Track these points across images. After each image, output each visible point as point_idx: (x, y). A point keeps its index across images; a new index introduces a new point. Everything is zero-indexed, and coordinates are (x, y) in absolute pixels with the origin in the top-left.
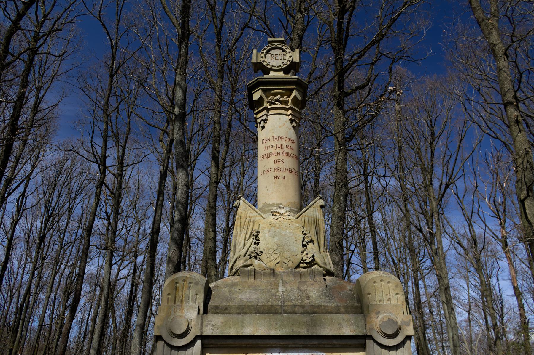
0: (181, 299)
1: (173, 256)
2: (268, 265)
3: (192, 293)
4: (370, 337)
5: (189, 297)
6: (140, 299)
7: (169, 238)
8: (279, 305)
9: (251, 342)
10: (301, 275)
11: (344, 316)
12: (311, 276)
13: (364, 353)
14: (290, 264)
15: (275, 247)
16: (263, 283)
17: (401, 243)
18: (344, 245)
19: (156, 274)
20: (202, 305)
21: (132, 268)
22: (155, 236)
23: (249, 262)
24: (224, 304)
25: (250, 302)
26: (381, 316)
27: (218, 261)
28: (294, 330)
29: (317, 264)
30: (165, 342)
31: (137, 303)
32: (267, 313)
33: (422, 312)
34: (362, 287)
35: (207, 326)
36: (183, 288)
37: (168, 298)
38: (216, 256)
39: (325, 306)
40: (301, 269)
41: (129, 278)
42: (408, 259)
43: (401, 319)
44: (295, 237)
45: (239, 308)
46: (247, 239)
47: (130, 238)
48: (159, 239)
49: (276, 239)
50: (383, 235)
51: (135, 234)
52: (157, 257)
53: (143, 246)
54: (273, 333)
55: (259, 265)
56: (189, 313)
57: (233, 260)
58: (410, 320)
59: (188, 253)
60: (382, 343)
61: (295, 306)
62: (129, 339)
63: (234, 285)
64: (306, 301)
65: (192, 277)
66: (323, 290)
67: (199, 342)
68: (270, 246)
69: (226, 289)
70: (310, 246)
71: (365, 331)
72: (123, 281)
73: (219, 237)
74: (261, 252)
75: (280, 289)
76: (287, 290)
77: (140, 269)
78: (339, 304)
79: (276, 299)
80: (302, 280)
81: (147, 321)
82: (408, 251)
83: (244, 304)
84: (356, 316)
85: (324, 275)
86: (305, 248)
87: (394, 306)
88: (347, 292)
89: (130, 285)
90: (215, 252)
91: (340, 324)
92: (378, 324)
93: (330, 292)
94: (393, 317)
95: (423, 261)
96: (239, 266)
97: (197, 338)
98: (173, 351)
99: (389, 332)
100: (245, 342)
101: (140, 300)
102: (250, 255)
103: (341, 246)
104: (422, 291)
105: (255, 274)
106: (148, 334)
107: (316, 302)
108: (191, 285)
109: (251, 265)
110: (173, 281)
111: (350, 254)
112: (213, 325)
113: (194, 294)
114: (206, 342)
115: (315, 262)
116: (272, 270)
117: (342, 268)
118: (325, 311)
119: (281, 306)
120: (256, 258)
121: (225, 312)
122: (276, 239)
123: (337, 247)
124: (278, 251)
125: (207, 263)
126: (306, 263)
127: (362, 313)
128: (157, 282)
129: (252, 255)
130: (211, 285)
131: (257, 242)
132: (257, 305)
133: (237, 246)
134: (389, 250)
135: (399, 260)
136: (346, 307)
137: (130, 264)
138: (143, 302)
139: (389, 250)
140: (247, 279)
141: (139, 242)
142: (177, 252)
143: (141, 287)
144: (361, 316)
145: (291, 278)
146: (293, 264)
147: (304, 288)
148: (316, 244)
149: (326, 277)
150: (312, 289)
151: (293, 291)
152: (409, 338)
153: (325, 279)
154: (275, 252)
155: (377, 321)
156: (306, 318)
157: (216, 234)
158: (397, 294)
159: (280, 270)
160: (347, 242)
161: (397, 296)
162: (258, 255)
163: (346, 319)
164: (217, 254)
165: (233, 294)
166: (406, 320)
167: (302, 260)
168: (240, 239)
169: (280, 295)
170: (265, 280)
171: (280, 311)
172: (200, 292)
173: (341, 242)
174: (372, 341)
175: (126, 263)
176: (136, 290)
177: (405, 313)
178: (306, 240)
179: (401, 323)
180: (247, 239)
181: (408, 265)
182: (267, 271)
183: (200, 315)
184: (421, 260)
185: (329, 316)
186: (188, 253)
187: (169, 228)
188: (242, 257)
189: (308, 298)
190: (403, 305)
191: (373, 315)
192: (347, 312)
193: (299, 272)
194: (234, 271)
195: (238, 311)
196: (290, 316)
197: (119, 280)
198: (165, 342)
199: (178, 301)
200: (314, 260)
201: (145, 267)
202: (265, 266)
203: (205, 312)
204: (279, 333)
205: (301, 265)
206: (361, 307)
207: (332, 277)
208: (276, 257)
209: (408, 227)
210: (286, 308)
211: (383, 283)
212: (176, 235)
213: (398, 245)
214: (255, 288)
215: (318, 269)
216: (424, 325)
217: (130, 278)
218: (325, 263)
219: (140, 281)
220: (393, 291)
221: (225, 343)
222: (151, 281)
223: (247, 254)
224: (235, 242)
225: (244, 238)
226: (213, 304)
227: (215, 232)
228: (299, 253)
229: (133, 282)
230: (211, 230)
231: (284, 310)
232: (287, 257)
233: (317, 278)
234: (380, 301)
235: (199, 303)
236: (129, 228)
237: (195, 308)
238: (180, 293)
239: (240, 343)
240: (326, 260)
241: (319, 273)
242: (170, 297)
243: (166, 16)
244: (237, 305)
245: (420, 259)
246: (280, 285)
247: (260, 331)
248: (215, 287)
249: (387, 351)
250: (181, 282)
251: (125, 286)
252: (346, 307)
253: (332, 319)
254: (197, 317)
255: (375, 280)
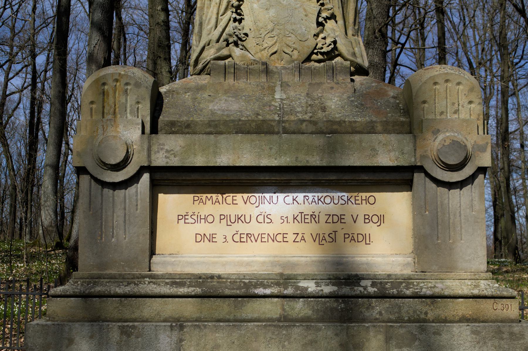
0: (112, 110)
1: (96, 51)
2: (257, 57)
3: (131, 100)
4: (421, 169)
5: (126, 107)
6: (47, 127)
7: (87, 25)
8: (275, 121)
9: (229, 176)
10: (313, 72)
11: (381, 137)
12: (330, 74)
13: (409, 193)
14: (295, 54)
15: (270, 26)
16: (247, 85)
17: (485, 34)
18: (389, 34)
19: (70, 86)
20: (148, 119)
21: (29, 76)
22: (64, 19)
23: (225, 52)
24: (185, 118)
25: (228, 116)
26: (441, 137)
27: (174, 63)
28: (299, 159)
29: (340, 55)
30: (92, 177)
31: (44, 133)
32: (256, 133)
33: (508, 146)
34: (414, 91)
35: (158, 152)
36: (115, 93)
37: (91, 109)
38: (169, 53)
39: (350, 122)
40: (312, 63)
41: (25, 92)
42: (495, 61)
43: (472, 142)
44: (305, 10)
45: (209, 124)
46: (220, 14)
47: (19, 25)
48: (71, 25)
49: (272, 12)
50: (456, 20)
51: (27, 17)
52: (69, 58)
53: (44, 37)
54: (265, 162)
55: (243, 57)
56: (128, 133)
57: (198, 50)
58: (487, 143)
59: (122, 49)
60: (439, 177)
61: (302, 121)
62: (35, 189)
63: (200, 88)
64: (320, 114)
65: (129, 74)
66: (349, 97)
67: (146, 177)
68: (260, 25)
69: (188, 96)
70: (330, 25)
71: (413, 160)
72: (16, 96)
73: (174, 23)
74: (246, 35)
75: (277, 96)
76: (291, 97)
77: (42, 77)
78: (374, 119)
79: (270, 110)
80: (314, 82)
81: (62, 159)
82: (495, 48)
83: (217, 118)
84: (401, 136)
85: (352, 74)
86: (321, 27)
87: (465, 121)
88: (388, 101)
89: (28, 105)
90: (169, 47)
91: (373, 149)
92: (435, 149)
93: (361, 100)
94: (460, 138)
95: (519, 65)
96: (209, 58)
97: (142, 170)
98: (106, 190)
99: (453, 161)
100: (221, 176)
101: (47, 128)
102: (226, 40)
103: (384, 36)
104: (512, 116)
105: (236, 71)
106: (65, 180)
107: (337, 116)
108: (129, 87)
109: (229, 56)
110: (97, 81)
111: (398, 51)
112: (167, 151)
113: (134, 103)
114: (158, 176)
115: (337, 53)
116: (265, 64)
117: (383, 65)
118: (350, 130)
119: (279, 121)
120: (236, 44)
121: (187, 130)
122: (272, 12)
123: (376, 37)
124: (274, 33)
125: (155, 63)
126: (322, 54)
127: (410, 132)
128: (73, 99)
129: (231, 40)
130: (163, 90)
131: (238, 17)
132: (240, 120)
133: (205, 26)
134: (464, 44)
135: (480, 64)
136: (386, 123)
137: (24, 69)
138: (53, 130)
139: (464, 44)
140: (222, 80)
141: (35, 32)
142: (103, 45)
143: (47, 107)
144: (408, 138)
145: (297, 79)
146: (299, 56)
147: (317, 93)
148: (340, 22)
149: (356, 78)
150: (330, 96)
151: (299, 99)
152: (482, 170)
153: (352, 80)
154: (268, 35)
155: (435, 144)
156: (319, 141)
157: (168, 15)
158: (470, 102)
159: (277, 65)
160: (393, 31)
161: (469, 106)
162: (240, 39)
163: (385, 142)
164: (173, 52)
165: (199, 103)
166: (481, 143)
167: (315, 48)
168: (209, 14)
169: (277, 104)
170: (253, 81)
171: (276, 130)
172: (144, 99)
173: (383, 29)
174: (423, 175)
175: (17, 67)
176: (39, 112)
177: (481, 132)
178: (324, 14)
179: (473, 148)
180: (220, 14)
181: (495, 71)
182: (255, 67)
183: (146, 136)
184: (517, 64)
185: (357, 137)
186: (122, 49)
187: (87, 7)
188: (213, 43)
189: (324, 109)
190: (478, 119)
191: (429, 136)
192: (386, 131)
193: (309, 68)
194: (200, 66)
195: (208, 130)
196: (294, 136)
197: (10, 94)
198: (92, 177)
199: (108, 113)
200: (335, 48)
201: (50, 74)
202: (252, 58)
203: (154, 130)
204: (274, 163)
205: (314, 57)
206: (410, 124)
207: (366, 77)
208: (270, 43)
209: (502, 5)
210: (287, 125)
211: (449, 85)
212: (98, 15)
213: (480, 37)
214: (236, 94)
215: (342, 64)
216: (509, 166)
217: (27, 92)
218: (354, 54)
219: (45, 98)
220: (464, 97)
221: (188, 178)
222: (63, 99)
223: (222, 39)
224: (201, 18)
225: (215, 11)
226: (167, 119)
227: (166, 11)
228: (311, 37)
229: (33, 99)
230: (159, 8)
231: (284, 128)
232: (290, 44)
233: (340, 78)
234: (442, 113)
235: (143, 116)
236: (17, 6)
237: (138, 124)
238: (111, 100)
239: (212, 178)
240: (354, 48)
241: (343, 70)
242: (94, 106)
243: (170, 277)
244: (206, 119)
245: (516, 61)
246: (278, 89)
247: (244, 160)
248: (169, 91)
249: (446, 190)
250: (110, 82)
251: (21, 106)
252: (386, 123)
253: (361, 141)
254: (141, 138)
255: (437, 81)
